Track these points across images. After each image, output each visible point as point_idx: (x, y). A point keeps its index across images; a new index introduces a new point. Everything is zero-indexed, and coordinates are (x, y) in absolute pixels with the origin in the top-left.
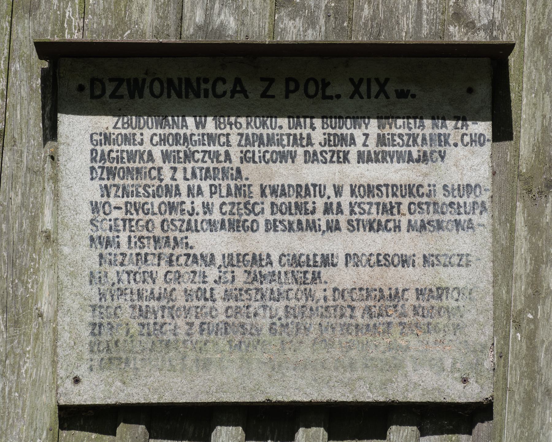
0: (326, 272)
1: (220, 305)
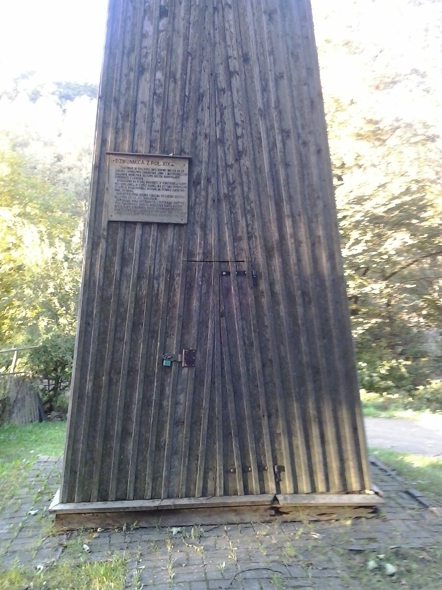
0: (158, 198)
1: (138, 203)
